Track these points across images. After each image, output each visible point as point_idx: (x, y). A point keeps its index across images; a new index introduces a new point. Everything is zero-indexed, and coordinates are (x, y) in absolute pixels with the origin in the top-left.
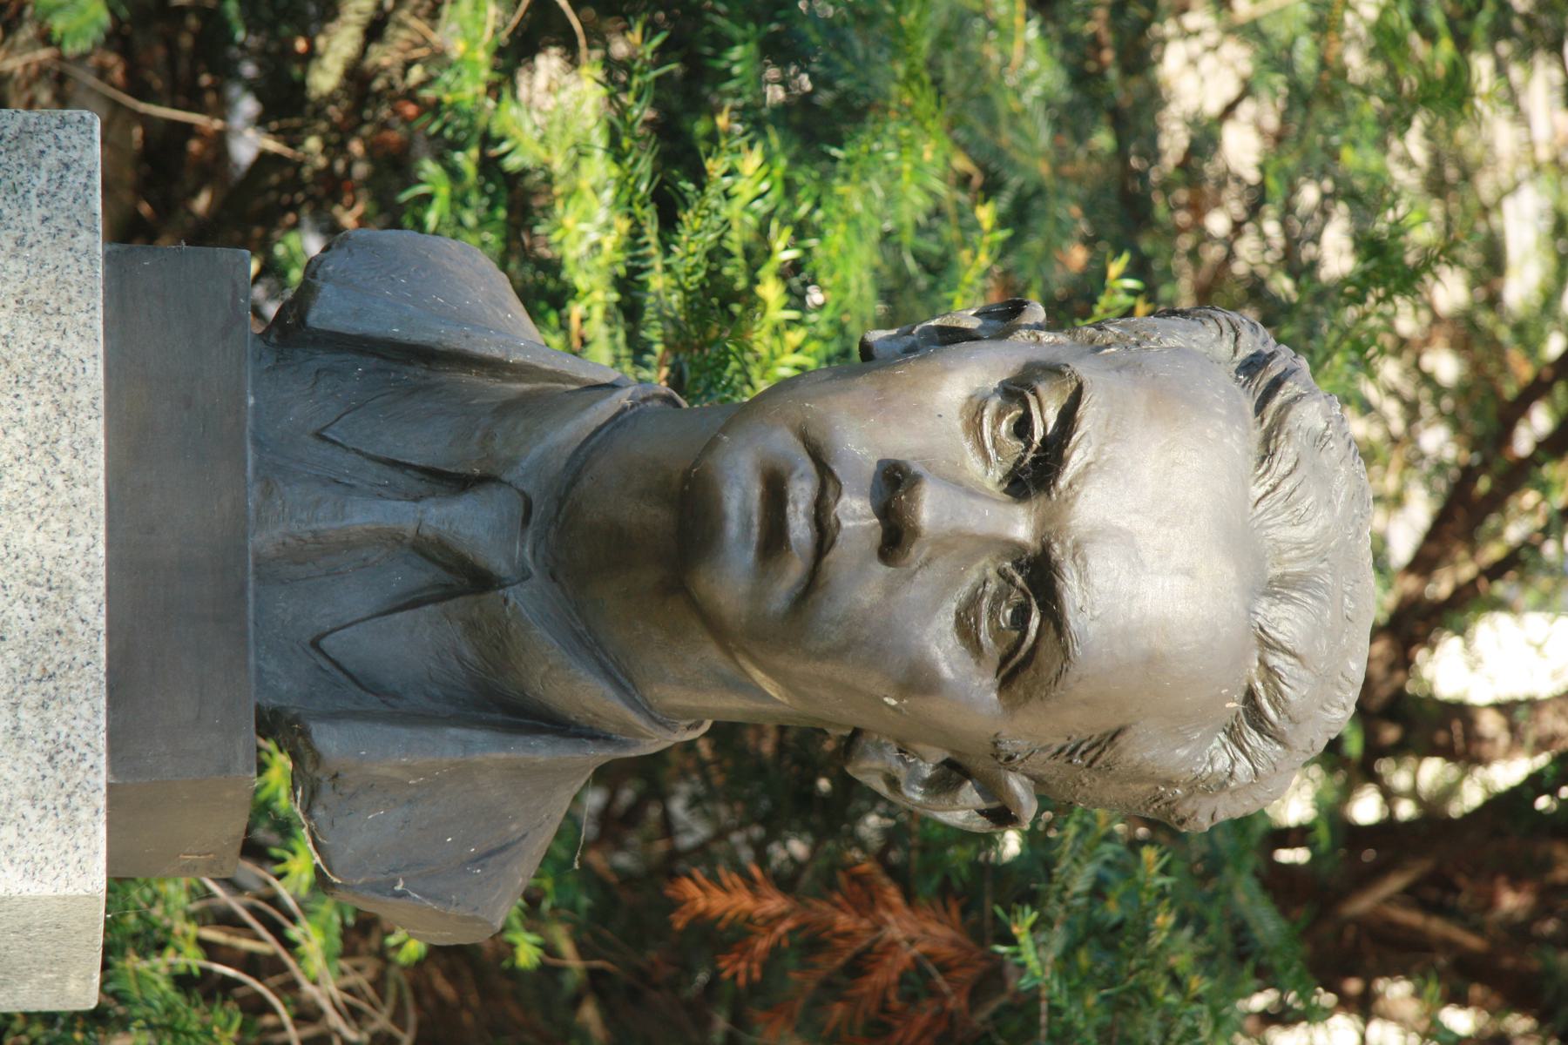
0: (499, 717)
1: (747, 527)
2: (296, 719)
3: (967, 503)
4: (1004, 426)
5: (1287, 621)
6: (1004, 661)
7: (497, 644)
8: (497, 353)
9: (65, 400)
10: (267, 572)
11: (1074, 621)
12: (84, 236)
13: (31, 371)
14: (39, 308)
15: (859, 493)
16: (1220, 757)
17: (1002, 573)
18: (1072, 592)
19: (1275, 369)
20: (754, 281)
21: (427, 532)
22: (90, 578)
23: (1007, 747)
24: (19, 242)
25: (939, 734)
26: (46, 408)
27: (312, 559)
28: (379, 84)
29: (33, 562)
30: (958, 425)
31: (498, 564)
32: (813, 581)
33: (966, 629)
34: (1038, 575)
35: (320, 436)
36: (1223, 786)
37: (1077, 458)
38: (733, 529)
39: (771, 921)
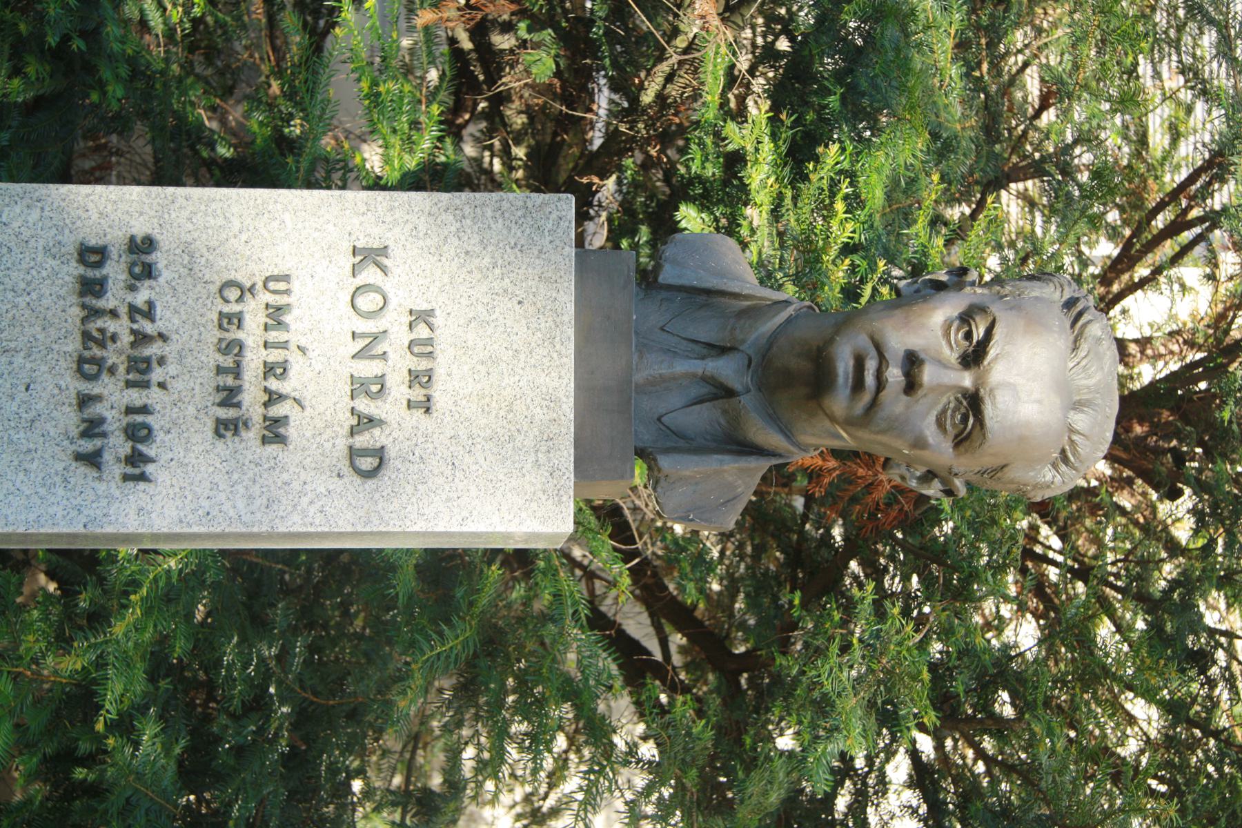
0: (734, 447)
1: (847, 379)
2: (651, 453)
3: (944, 376)
4: (960, 335)
5: (1080, 420)
6: (956, 436)
7: (735, 420)
8: (737, 290)
9: (558, 320)
10: (641, 390)
11: (989, 423)
12: (567, 249)
13: (544, 308)
14: (548, 280)
15: (896, 366)
16: (1048, 474)
17: (957, 399)
18: (988, 410)
19: (1080, 306)
20: (832, 203)
21: (708, 374)
22: (568, 397)
23: (955, 470)
24: (540, 252)
25: (923, 463)
26: (550, 323)
27: (657, 385)
28: (670, 101)
29: (544, 390)
30: (940, 333)
31: (737, 386)
32: (874, 403)
33: (940, 423)
34: (973, 402)
35: (662, 329)
36: (1048, 487)
37: (992, 352)
38: (841, 380)
39: (830, 471)
